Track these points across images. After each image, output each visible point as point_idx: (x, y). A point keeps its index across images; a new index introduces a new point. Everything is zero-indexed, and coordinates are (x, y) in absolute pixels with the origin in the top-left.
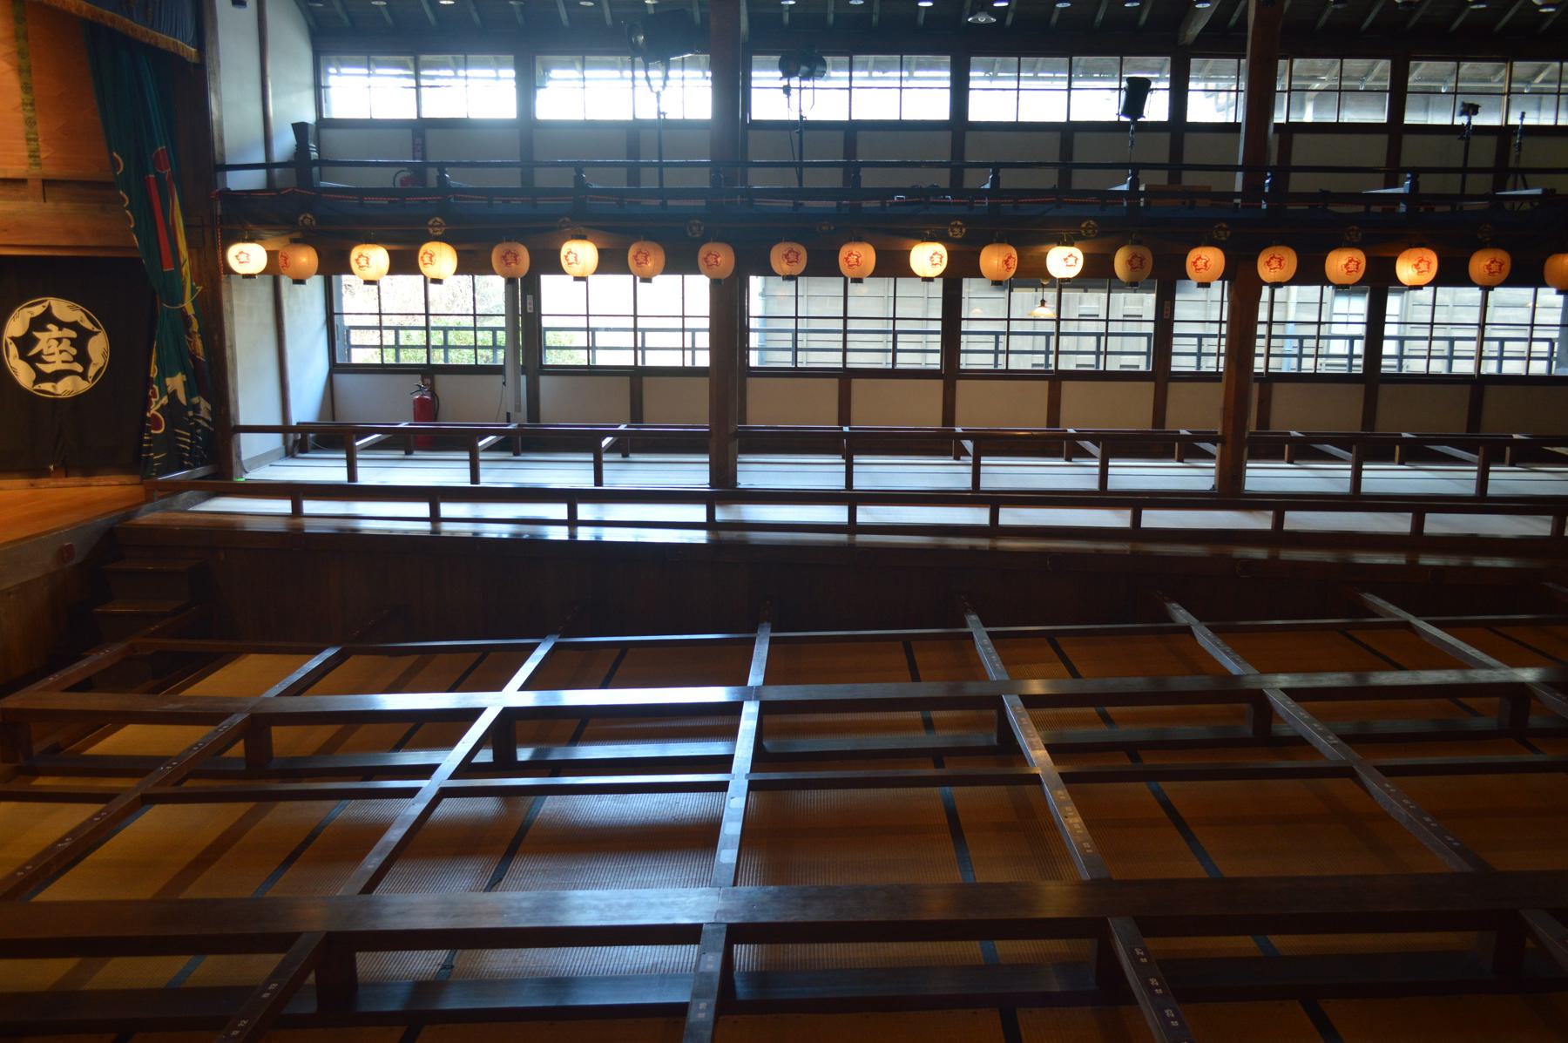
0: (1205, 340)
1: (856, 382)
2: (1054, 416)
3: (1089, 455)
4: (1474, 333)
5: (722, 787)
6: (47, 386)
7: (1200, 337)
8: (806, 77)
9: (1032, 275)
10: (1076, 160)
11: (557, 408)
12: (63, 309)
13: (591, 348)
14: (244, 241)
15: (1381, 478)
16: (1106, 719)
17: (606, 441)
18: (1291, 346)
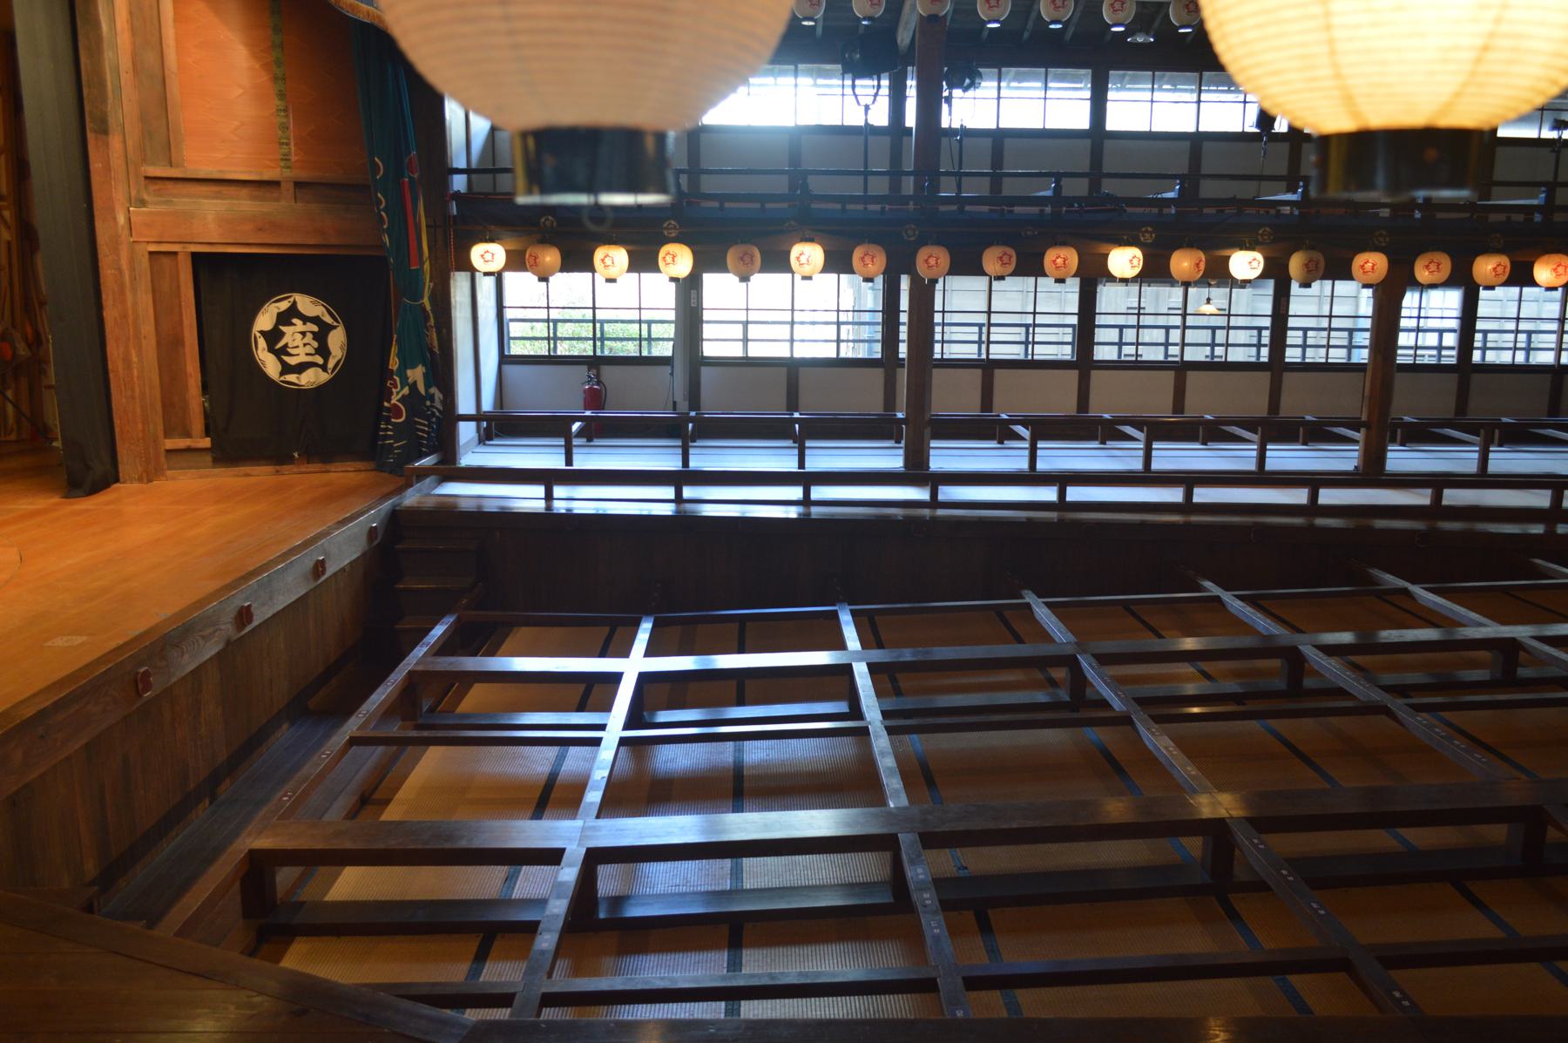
0: (1310, 334)
1: (998, 373)
2: (987, 402)
3: (1020, 438)
4: (1554, 326)
5: (596, 742)
6: (292, 378)
7: (1121, 328)
8: (966, 89)
9: (1217, 274)
10: (1204, 171)
11: (1298, 402)
12: (307, 304)
13: (553, 339)
14: (486, 241)
15: (1283, 457)
16: (1207, 676)
17: (576, 426)
18: (1113, 335)
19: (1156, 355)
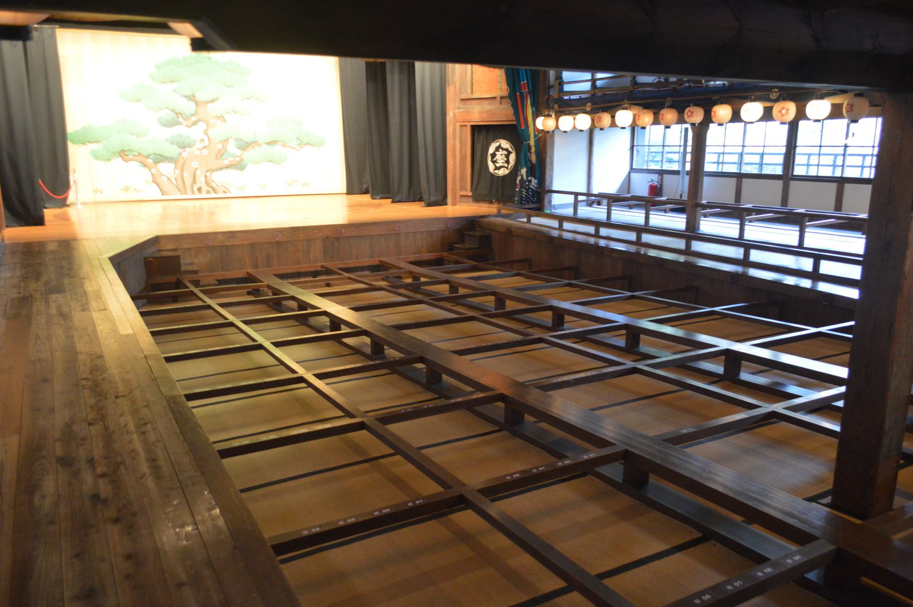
7: (809, 155)
13: (761, 165)
19: (826, 172)
